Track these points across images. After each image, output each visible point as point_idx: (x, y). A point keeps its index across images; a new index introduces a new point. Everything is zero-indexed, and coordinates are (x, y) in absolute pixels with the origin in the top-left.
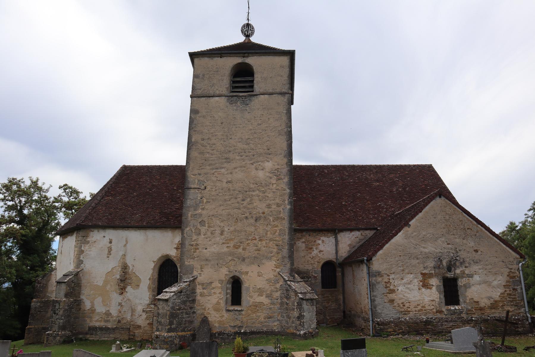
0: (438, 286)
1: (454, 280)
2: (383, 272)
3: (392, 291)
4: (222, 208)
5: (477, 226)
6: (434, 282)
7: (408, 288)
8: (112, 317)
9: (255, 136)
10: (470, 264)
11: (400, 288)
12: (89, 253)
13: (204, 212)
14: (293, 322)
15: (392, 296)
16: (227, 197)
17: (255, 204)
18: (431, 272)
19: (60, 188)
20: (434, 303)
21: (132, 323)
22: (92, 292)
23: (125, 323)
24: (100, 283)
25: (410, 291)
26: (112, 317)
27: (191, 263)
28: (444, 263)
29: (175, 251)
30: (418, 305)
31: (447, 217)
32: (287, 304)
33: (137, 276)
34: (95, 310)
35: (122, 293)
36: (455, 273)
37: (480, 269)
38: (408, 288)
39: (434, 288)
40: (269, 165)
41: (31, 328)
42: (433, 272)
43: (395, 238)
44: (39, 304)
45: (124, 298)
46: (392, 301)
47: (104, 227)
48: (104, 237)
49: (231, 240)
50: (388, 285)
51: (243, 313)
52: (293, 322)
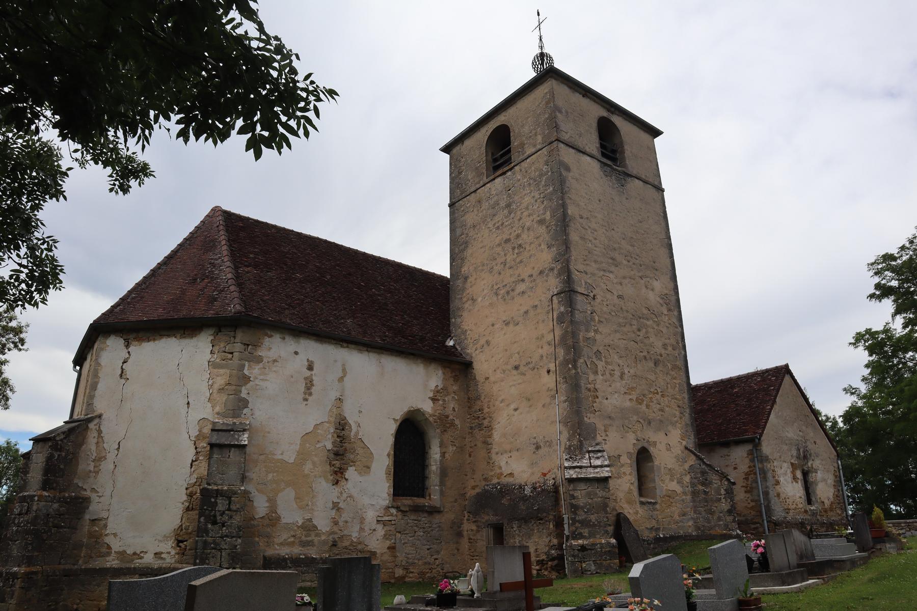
4: (618, 335)
8: (318, 535)
12: (261, 383)
13: (598, 337)
14: (719, 519)
21: (359, 547)
22: (270, 476)
23: (346, 548)
24: (290, 457)
26: (318, 535)
27: (592, 420)
29: (431, 402)
32: (705, 493)
33: (365, 447)
34: (279, 518)
35: (337, 483)
41: (35, 573)
44: (56, 506)
45: (341, 493)
47: (298, 332)
48: (296, 353)
49: (633, 389)
51: (658, 506)
52: (719, 519)
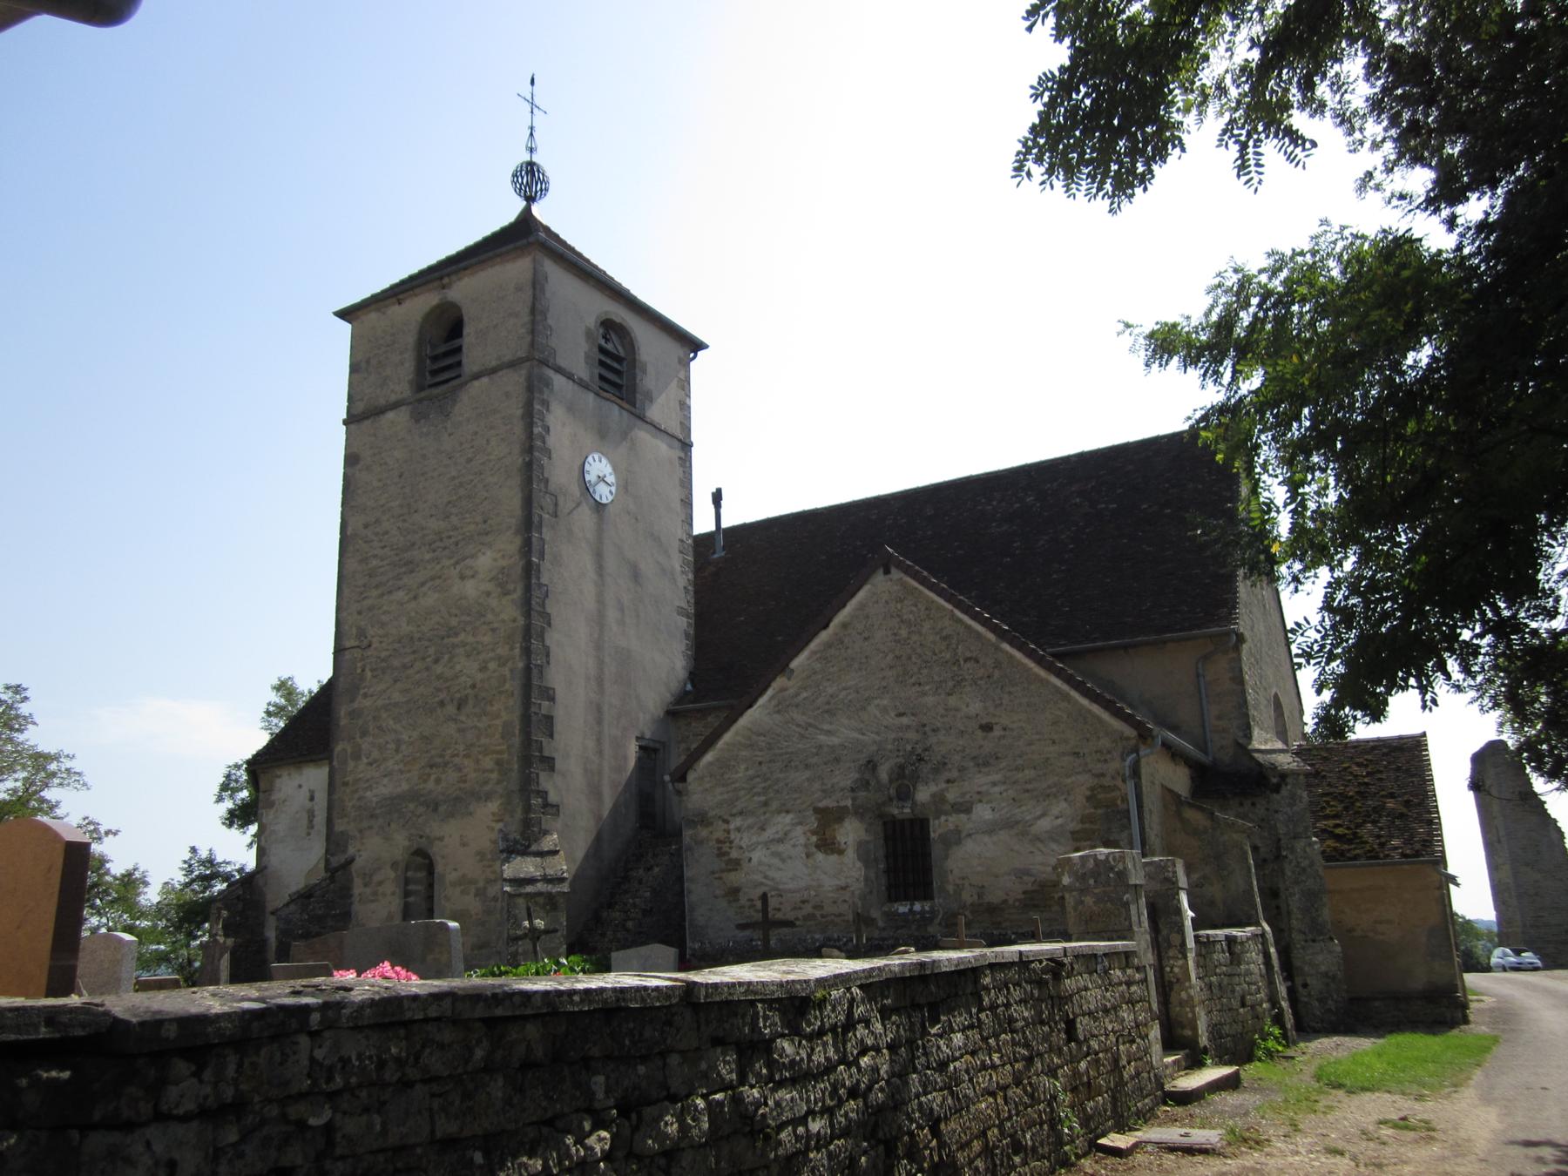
0: (861, 847)
1: (919, 827)
2: (712, 813)
3: (735, 865)
5: (997, 648)
6: (850, 833)
7: (776, 854)
9: (462, 492)
10: (962, 769)
11: (757, 856)
15: (734, 878)
16: (407, 660)
17: (458, 667)
18: (842, 804)
19: (8, 688)
20: (847, 896)
25: (783, 861)
28: (884, 774)
30: (803, 902)
31: (904, 633)
36: (914, 803)
37: (994, 784)
38: (776, 854)
39: (851, 854)
40: (485, 561)
42: (849, 803)
43: (750, 712)
46: (734, 893)
50: (725, 848)
